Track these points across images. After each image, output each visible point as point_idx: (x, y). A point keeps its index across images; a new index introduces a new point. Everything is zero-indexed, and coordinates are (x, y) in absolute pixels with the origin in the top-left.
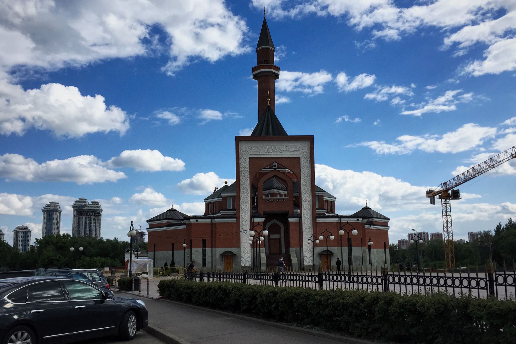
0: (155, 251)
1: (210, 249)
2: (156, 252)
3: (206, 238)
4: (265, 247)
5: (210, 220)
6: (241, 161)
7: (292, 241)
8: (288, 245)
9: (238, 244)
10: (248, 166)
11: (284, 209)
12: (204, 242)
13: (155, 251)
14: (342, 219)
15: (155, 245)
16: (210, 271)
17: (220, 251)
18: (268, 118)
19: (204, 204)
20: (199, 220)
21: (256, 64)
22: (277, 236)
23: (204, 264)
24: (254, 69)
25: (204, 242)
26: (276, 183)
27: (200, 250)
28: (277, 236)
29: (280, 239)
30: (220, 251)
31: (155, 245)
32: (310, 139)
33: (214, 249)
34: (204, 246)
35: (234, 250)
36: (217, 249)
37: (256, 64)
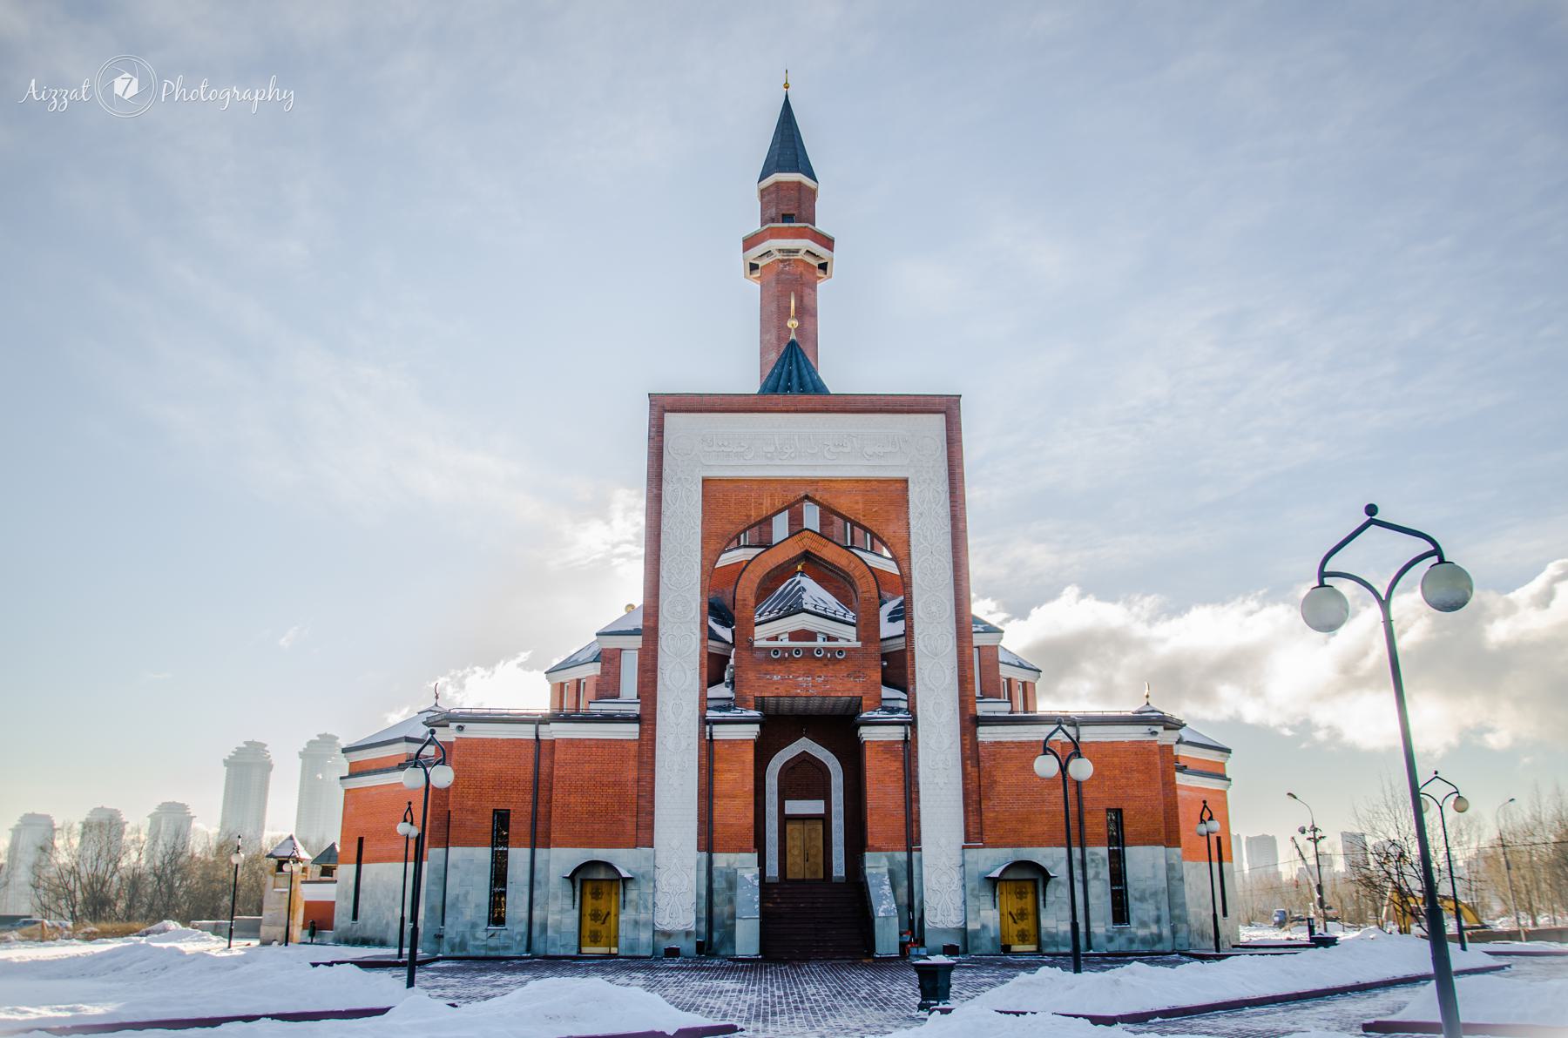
0: (359, 862)
1: (527, 851)
2: (364, 866)
3: (511, 807)
4: (760, 845)
5: (532, 727)
6: (668, 489)
7: (875, 827)
8: (857, 844)
9: (642, 833)
10: (699, 530)
11: (835, 688)
12: (502, 819)
13: (359, 862)
14: (1083, 730)
15: (361, 840)
16: (518, 950)
17: (561, 860)
18: (790, 373)
19: (548, 687)
20: (468, 726)
21: (756, 226)
22: (815, 807)
23: (497, 919)
24: (749, 243)
25: (502, 819)
26: (813, 592)
27: (484, 854)
28: (815, 807)
29: (825, 819)
30: (561, 860)
31: (361, 840)
32: (947, 408)
33: (541, 853)
34: (1117, 842)
35: (624, 860)
36: (455, 853)
37: (756, 226)
